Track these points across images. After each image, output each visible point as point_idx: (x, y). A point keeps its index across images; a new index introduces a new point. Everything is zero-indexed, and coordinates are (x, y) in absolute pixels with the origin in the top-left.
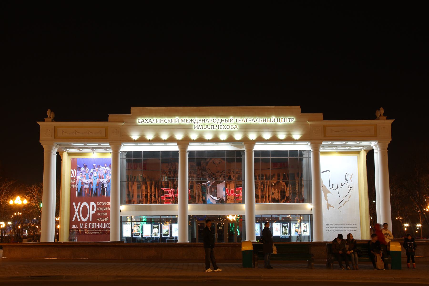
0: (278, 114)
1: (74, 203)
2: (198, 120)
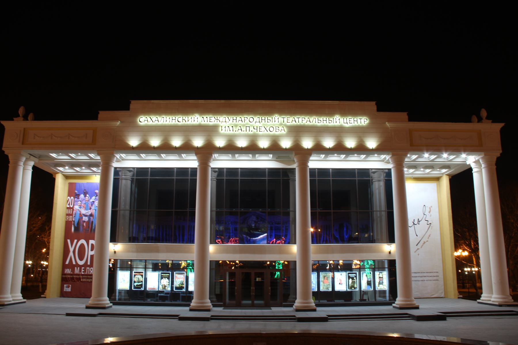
0: (344, 113)
1: (69, 241)
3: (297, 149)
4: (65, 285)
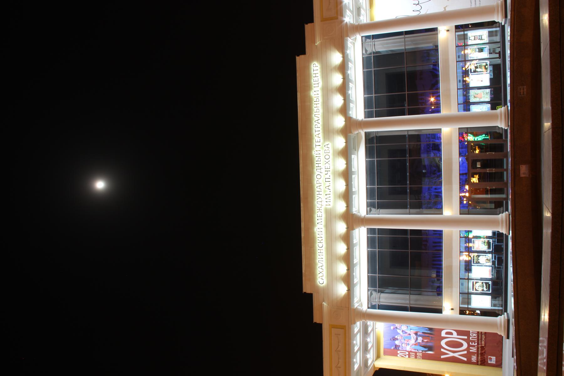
0: (308, 87)
1: (442, 357)
3: (346, 131)
4: (489, 362)
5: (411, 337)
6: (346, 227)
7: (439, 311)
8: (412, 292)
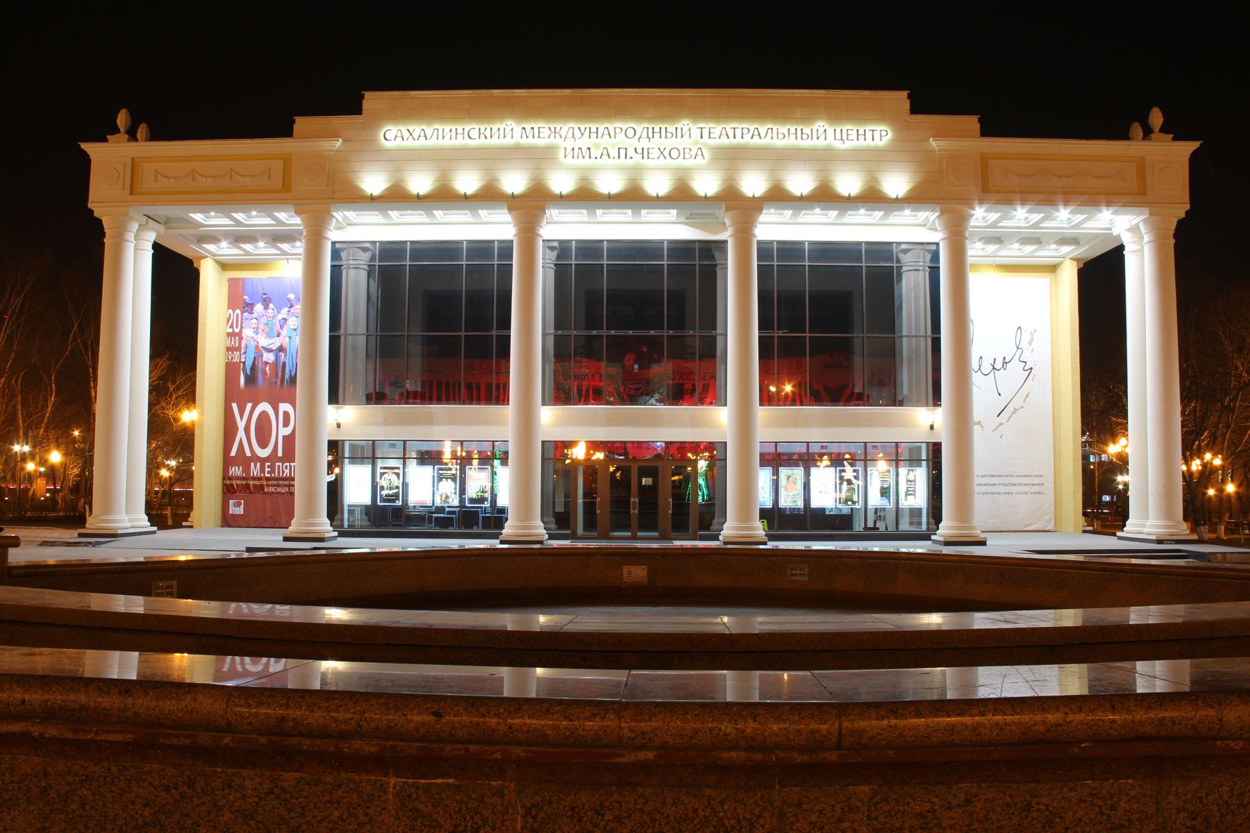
0: (836, 115)
1: (234, 406)
2: (576, 130)
3: (730, 198)
5: (272, 337)
6: (516, 193)
7: (334, 398)
8: (372, 339)
